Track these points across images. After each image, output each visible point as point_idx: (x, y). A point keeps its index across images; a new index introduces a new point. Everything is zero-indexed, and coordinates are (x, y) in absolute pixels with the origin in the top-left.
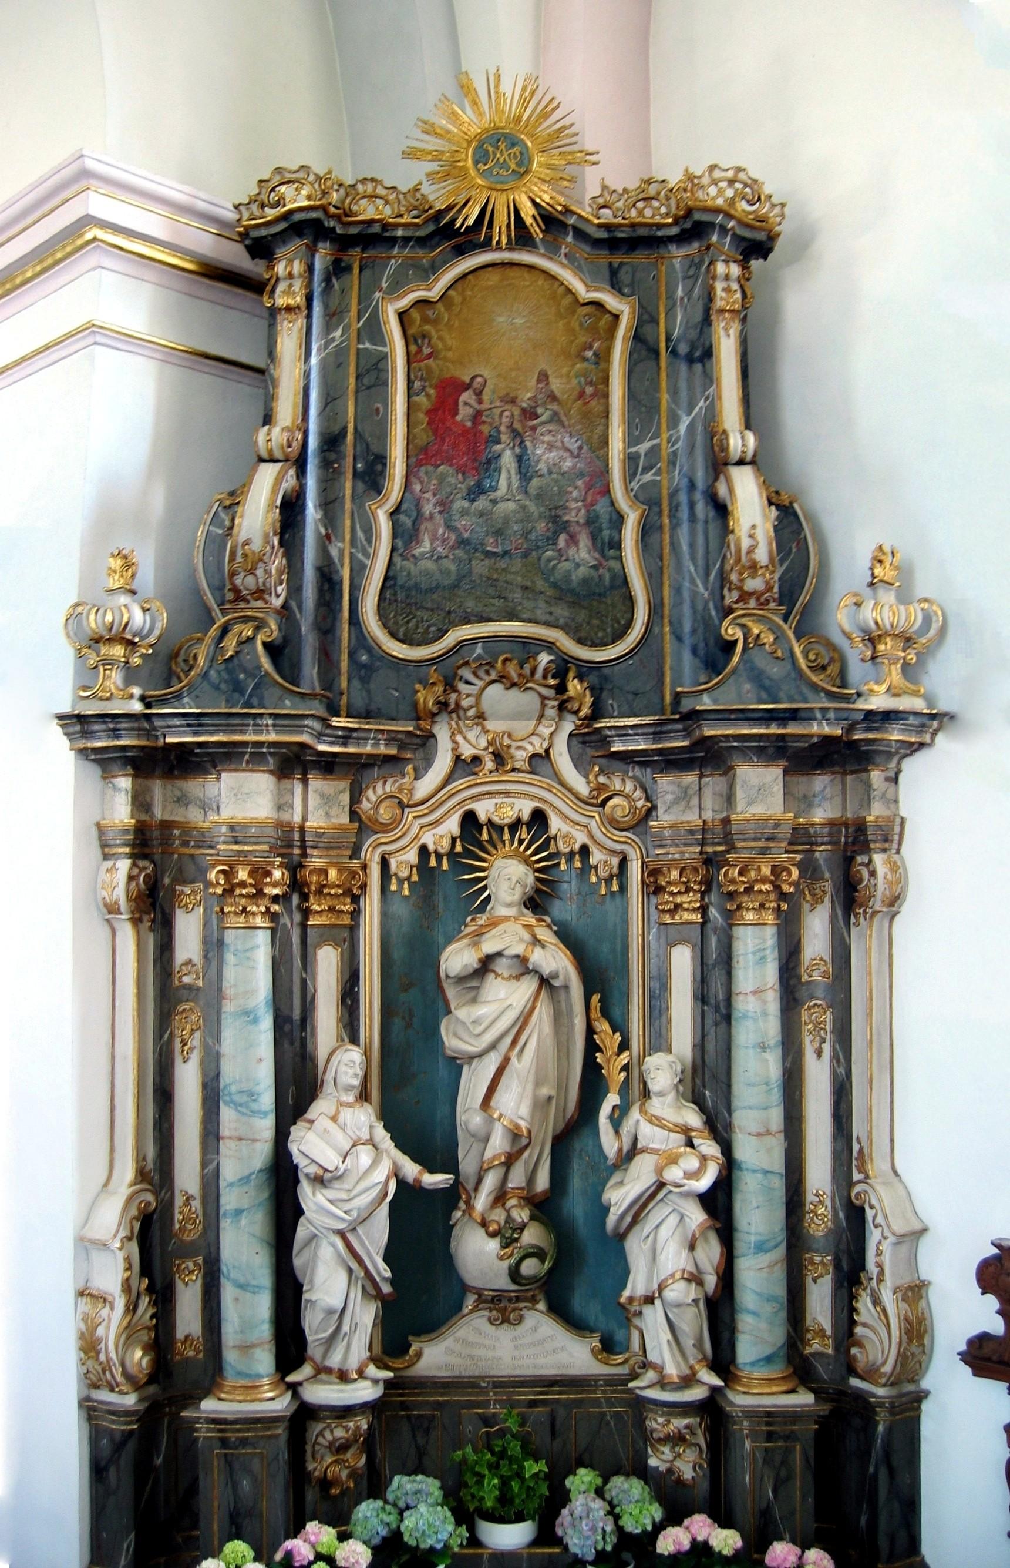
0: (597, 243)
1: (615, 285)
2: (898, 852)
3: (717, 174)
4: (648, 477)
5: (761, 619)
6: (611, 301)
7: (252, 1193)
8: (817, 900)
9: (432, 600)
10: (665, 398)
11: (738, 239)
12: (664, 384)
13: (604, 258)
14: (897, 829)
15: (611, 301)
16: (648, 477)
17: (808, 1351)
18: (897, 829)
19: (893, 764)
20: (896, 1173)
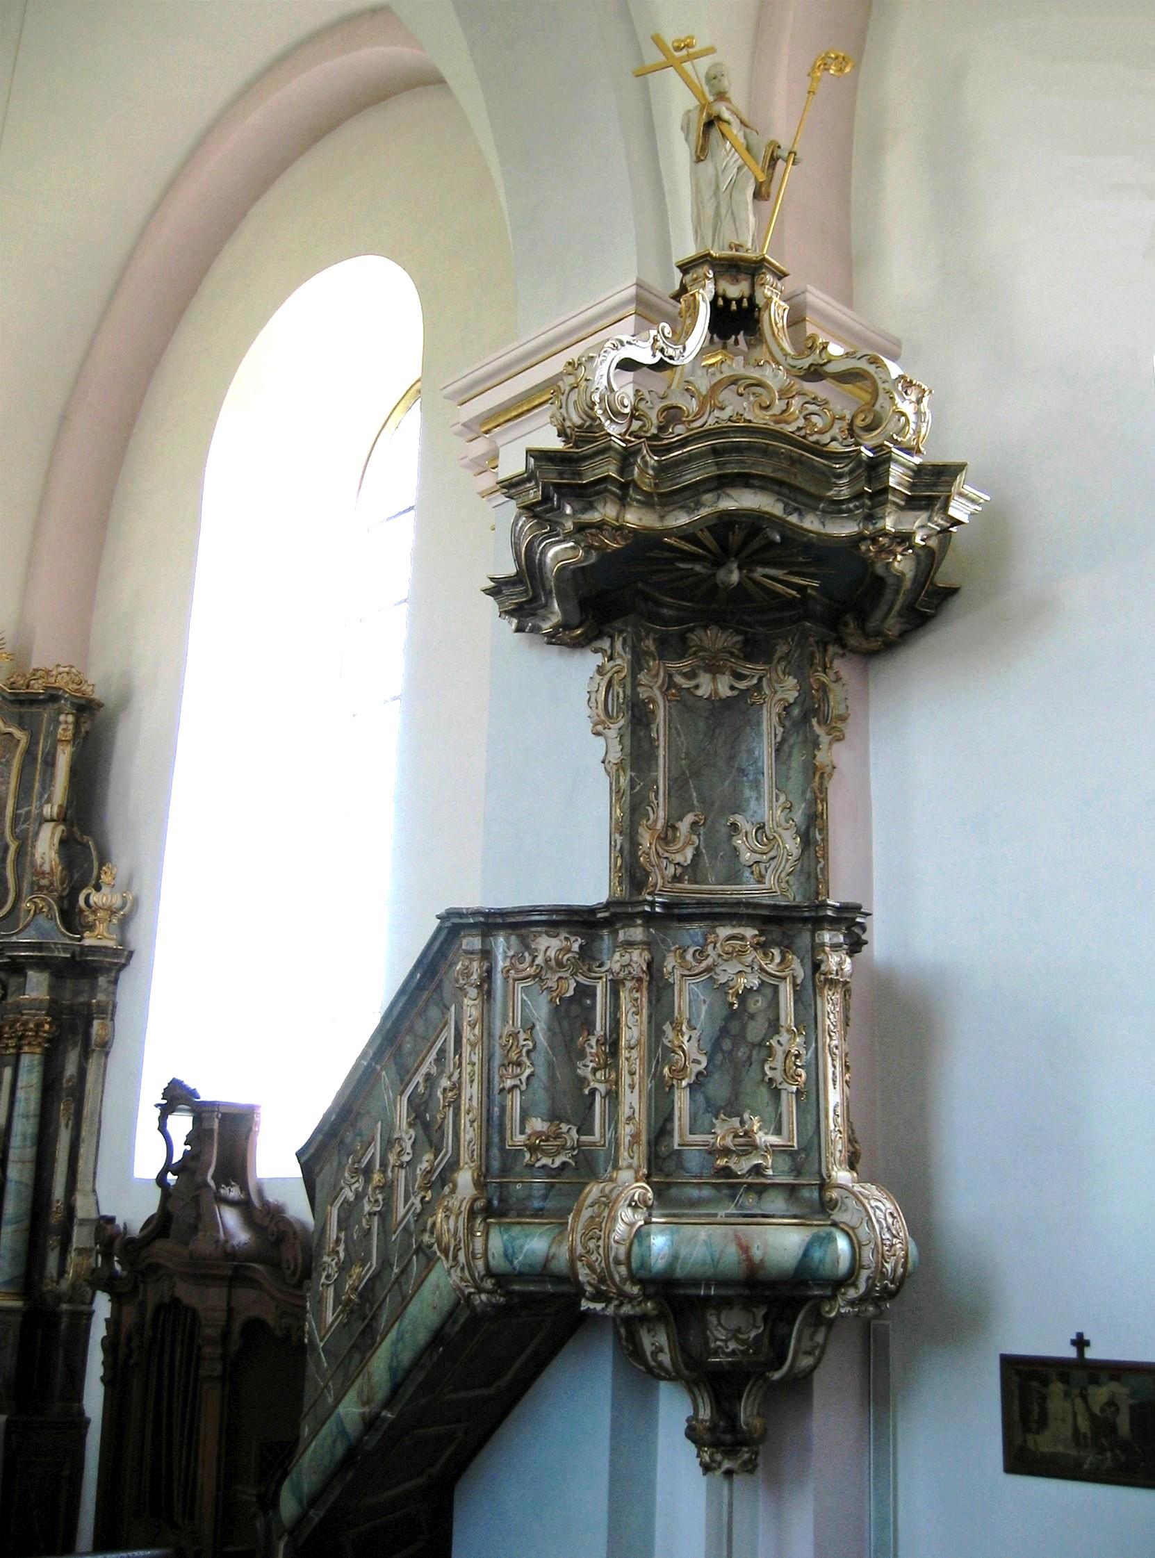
0: (12, 702)
1: (21, 726)
2: (112, 1020)
3: (61, 669)
4: (25, 826)
5: (43, 899)
6: (18, 733)
7: (672, 932)
8: (75, 1044)
9: (840, 964)
10: (37, 785)
11: (73, 704)
12: (37, 777)
13: (16, 709)
14: (110, 1008)
15: (18, 733)
16: (25, 826)
17: (45, 1289)
18: (110, 1008)
19: (113, 974)
20: (94, 1191)
